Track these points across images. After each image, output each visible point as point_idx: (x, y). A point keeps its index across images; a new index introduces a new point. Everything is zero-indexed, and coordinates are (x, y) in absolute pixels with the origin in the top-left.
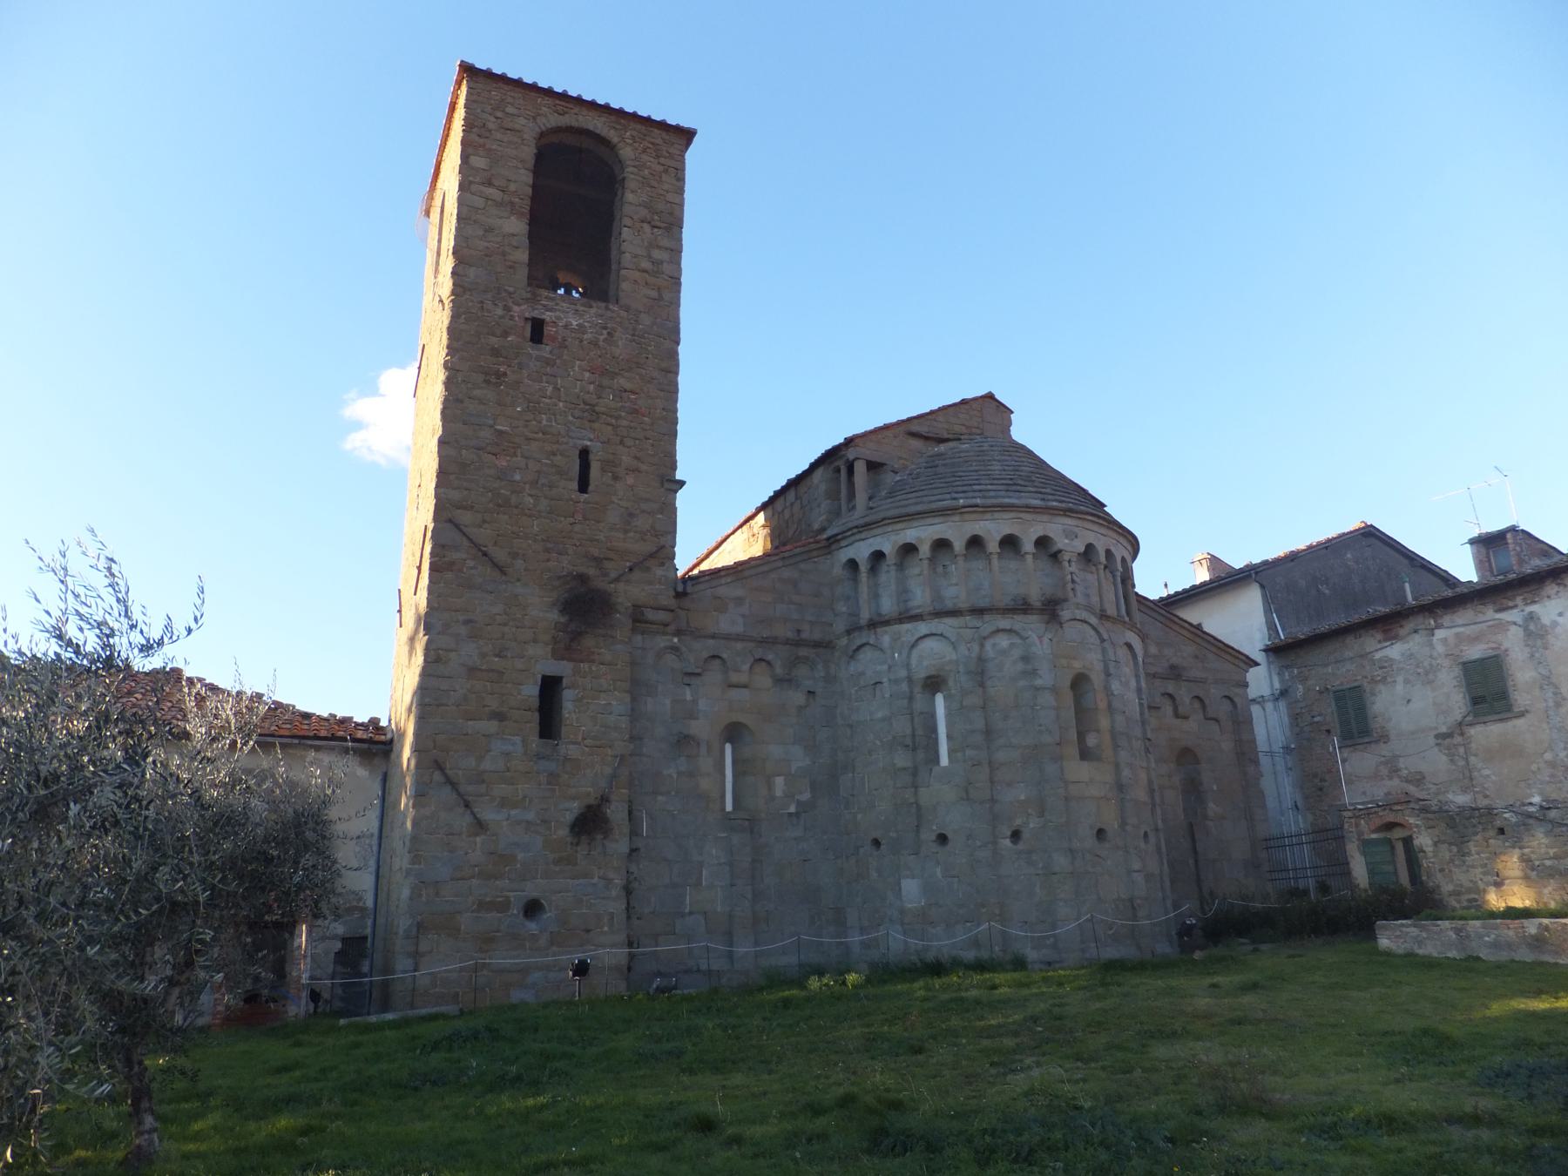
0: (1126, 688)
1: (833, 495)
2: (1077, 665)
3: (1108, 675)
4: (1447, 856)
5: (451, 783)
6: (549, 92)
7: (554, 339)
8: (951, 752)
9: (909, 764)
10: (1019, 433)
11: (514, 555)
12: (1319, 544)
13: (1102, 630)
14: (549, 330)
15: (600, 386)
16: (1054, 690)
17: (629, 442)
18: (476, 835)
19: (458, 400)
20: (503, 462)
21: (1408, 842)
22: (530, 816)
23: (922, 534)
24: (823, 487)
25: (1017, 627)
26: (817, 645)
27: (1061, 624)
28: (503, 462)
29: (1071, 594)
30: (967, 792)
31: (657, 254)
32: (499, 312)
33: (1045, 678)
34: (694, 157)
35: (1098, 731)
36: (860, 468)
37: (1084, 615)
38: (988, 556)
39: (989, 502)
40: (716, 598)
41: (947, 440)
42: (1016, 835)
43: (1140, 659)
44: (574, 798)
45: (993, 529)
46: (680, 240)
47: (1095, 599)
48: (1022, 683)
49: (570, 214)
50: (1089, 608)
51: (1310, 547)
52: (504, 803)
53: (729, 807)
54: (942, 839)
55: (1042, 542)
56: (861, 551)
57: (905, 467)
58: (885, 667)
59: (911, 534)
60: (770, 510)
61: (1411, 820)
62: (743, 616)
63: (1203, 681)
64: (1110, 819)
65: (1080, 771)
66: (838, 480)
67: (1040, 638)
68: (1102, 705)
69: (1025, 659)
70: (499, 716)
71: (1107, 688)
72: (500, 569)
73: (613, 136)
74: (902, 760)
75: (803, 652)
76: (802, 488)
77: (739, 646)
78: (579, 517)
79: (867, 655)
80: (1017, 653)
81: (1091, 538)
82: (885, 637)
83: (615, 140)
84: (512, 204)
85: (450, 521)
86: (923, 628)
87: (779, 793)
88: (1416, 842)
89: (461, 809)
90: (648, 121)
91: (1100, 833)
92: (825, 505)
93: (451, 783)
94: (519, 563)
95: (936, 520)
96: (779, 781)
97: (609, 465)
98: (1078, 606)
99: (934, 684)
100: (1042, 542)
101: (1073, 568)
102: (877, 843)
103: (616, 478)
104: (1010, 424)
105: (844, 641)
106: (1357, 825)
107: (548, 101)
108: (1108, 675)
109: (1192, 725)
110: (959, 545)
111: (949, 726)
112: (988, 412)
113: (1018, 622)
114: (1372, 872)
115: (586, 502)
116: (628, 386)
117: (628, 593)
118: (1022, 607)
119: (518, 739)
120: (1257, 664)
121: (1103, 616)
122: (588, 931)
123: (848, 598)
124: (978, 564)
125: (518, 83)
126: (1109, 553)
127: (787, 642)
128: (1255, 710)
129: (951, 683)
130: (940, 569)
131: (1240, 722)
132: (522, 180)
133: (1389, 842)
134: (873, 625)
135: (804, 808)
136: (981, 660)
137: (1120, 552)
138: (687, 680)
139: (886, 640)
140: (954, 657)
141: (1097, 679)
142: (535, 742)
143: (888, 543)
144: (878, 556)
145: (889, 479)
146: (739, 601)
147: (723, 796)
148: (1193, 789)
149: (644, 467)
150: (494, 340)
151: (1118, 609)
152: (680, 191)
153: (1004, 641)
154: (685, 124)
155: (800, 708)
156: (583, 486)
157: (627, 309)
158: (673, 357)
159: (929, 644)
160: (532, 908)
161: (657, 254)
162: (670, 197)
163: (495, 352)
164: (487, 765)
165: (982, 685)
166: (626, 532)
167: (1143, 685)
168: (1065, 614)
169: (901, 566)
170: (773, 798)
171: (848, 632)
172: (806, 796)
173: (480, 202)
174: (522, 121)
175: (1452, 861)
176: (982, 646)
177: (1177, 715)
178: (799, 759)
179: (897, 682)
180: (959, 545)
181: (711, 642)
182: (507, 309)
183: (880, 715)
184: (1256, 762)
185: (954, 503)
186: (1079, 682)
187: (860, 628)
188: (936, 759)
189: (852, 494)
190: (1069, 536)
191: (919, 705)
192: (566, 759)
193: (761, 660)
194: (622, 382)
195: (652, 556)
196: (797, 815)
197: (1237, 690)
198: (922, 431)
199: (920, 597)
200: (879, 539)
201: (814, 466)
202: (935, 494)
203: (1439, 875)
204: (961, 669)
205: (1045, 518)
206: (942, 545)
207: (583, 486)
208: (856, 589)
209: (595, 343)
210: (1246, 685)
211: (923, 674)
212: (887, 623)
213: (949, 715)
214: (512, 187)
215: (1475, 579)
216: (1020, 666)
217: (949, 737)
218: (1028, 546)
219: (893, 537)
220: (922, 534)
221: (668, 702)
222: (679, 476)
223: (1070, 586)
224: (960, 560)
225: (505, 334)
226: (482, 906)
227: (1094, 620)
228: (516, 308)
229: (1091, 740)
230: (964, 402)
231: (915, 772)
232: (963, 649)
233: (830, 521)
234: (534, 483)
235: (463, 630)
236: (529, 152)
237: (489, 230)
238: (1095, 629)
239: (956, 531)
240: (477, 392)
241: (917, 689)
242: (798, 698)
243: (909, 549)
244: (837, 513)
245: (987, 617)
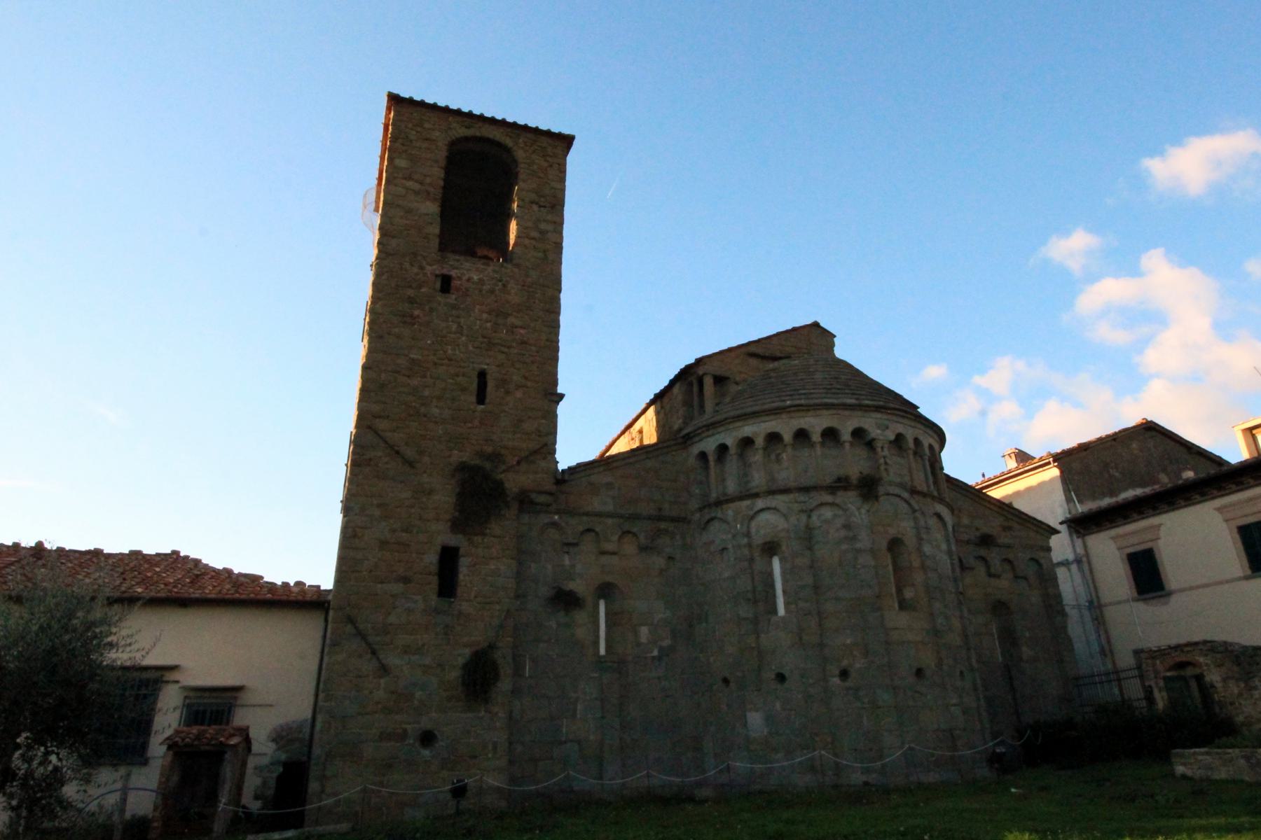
0: (938, 548)
1: (688, 403)
2: (892, 532)
3: (920, 539)
4: (1236, 691)
5: (361, 635)
6: (458, 112)
7: (458, 289)
8: (787, 604)
9: (751, 615)
10: (840, 352)
11: (421, 453)
12: (1108, 436)
13: (913, 502)
14: (456, 283)
15: (496, 324)
16: (873, 552)
17: (517, 366)
18: (380, 677)
19: (381, 337)
20: (415, 382)
21: (1199, 678)
22: (427, 661)
23: (757, 429)
24: (680, 398)
25: (838, 501)
26: (673, 520)
27: (877, 498)
28: (415, 382)
29: (884, 474)
30: (801, 638)
31: (543, 226)
32: (415, 270)
33: (864, 541)
34: (574, 160)
35: (913, 585)
36: (708, 382)
37: (897, 491)
38: (812, 445)
39: (812, 402)
40: (591, 484)
41: (780, 358)
42: (844, 674)
43: (950, 529)
44: (465, 646)
45: (816, 424)
47: (907, 479)
48: (844, 547)
50: (902, 485)
51: (1100, 439)
52: (406, 650)
53: (602, 651)
54: (781, 678)
55: (858, 433)
56: (709, 445)
57: (745, 380)
58: (730, 536)
59: (748, 430)
60: (659, 403)
61: (1201, 660)
62: (613, 498)
63: (1009, 547)
64: (928, 659)
65: (897, 620)
66: (691, 391)
67: (858, 509)
68: (916, 564)
69: (847, 527)
70: (406, 580)
71: (919, 550)
72: (411, 464)
73: (508, 142)
74: (745, 611)
75: (663, 525)
76: (666, 400)
77: (610, 521)
78: (476, 423)
79: (715, 525)
80: (839, 522)
81: (900, 429)
82: (730, 511)
84: (428, 193)
85: (369, 427)
86: (760, 503)
87: (644, 640)
88: (1208, 679)
89: (369, 656)
90: (536, 131)
91: (919, 673)
93: (361, 635)
94: (426, 459)
95: (767, 418)
96: (644, 631)
97: (503, 383)
98: (891, 483)
99: (771, 548)
100: (858, 433)
101: (886, 452)
102: (726, 681)
103: (508, 392)
104: (833, 345)
105: (698, 515)
106: (1154, 665)
107: (459, 119)
108: (920, 539)
109: (1004, 583)
110: (787, 437)
111: (785, 581)
112: (814, 338)
113: (841, 497)
114: (770, 564)
115: (483, 411)
116: (518, 323)
117: (514, 482)
118: (841, 484)
119: (419, 598)
120: (1056, 532)
121: (914, 492)
122: (475, 757)
123: (701, 483)
124: (806, 452)
125: (434, 107)
126: (917, 441)
127: (650, 518)
128: (1061, 573)
129: (784, 548)
130: (773, 457)
131: (1046, 577)
132: (435, 174)
133: (1183, 678)
134: (718, 503)
135: (664, 652)
136: (809, 529)
137: (927, 440)
138: (566, 549)
140: (786, 526)
141: (910, 540)
142: (434, 599)
143: (730, 438)
144: (723, 449)
145: (733, 389)
146: (609, 486)
147: (596, 643)
148: (1009, 637)
149: (529, 384)
150: (410, 292)
151: (928, 487)
152: (562, 180)
153: (828, 513)
154: (566, 131)
155: (661, 571)
156: (481, 399)
157: (518, 266)
159: (764, 517)
160: (427, 738)
163: (411, 301)
164: (392, 619)
165: (810, 549)
166: (514, 433)
167: (954, 548)
168: (881, 490)
169: (741, 455)
170: (639, 644)
171: (700, 510)
172: (666, 643)
173: (400, 190)
174: (437, 134)
175: (1240, 695)
176: (809, 517)
177: (990, 575)
178: (661, 613)
179: (739, 547)
180: (787, 437)
181: (585, 518)
182: (422, 268)
183: (726, 575)
184: (1063, 613)
185: (781, 404)
186: (895, 545)
187: (709, 506)
188: (774, 611)
189: (702, 406)
190: (880, 428)
191: (759, 565)
192: (460, 613)
193: (629, 532)
194: (511, 320)
195: (535, 452)
196: (659, 658)
197: (1042, 554)
198: (760, 353)
199: (758, 479)
200: (723, 435)
201: (673, 383)
202: (779, 406)
203: (1230, 708)
204: (792, 535)
205: (859, 413)
207: (481, 399)
208: (707, 476)
209: (492, 291)
210: (1049, 549)
211: (760, 541)
213: (783, 573)
214: (428, 180)
216: (843, 533)
217: (784, 592)
218: (846, 436)
219: (735, 434)
220: (757, 429)
221: (549, 567)
222: (560, 390)
223: (882, 468)
224: (789, 450)
225: (420, 287)
226: (384, 736)
227: (906, 495)
228: (429, 268)
229: (908, 594)
230: (794, 329)
231: (755, 621)
232: (793, 519)
235: (377, 513)
236: (442, 154)
237: (409, 211)
238: (906, 501)
239: (786, 427)
241: (756, 554)
242: (659, 562)
243: (747, 442)
245: (813, 494)
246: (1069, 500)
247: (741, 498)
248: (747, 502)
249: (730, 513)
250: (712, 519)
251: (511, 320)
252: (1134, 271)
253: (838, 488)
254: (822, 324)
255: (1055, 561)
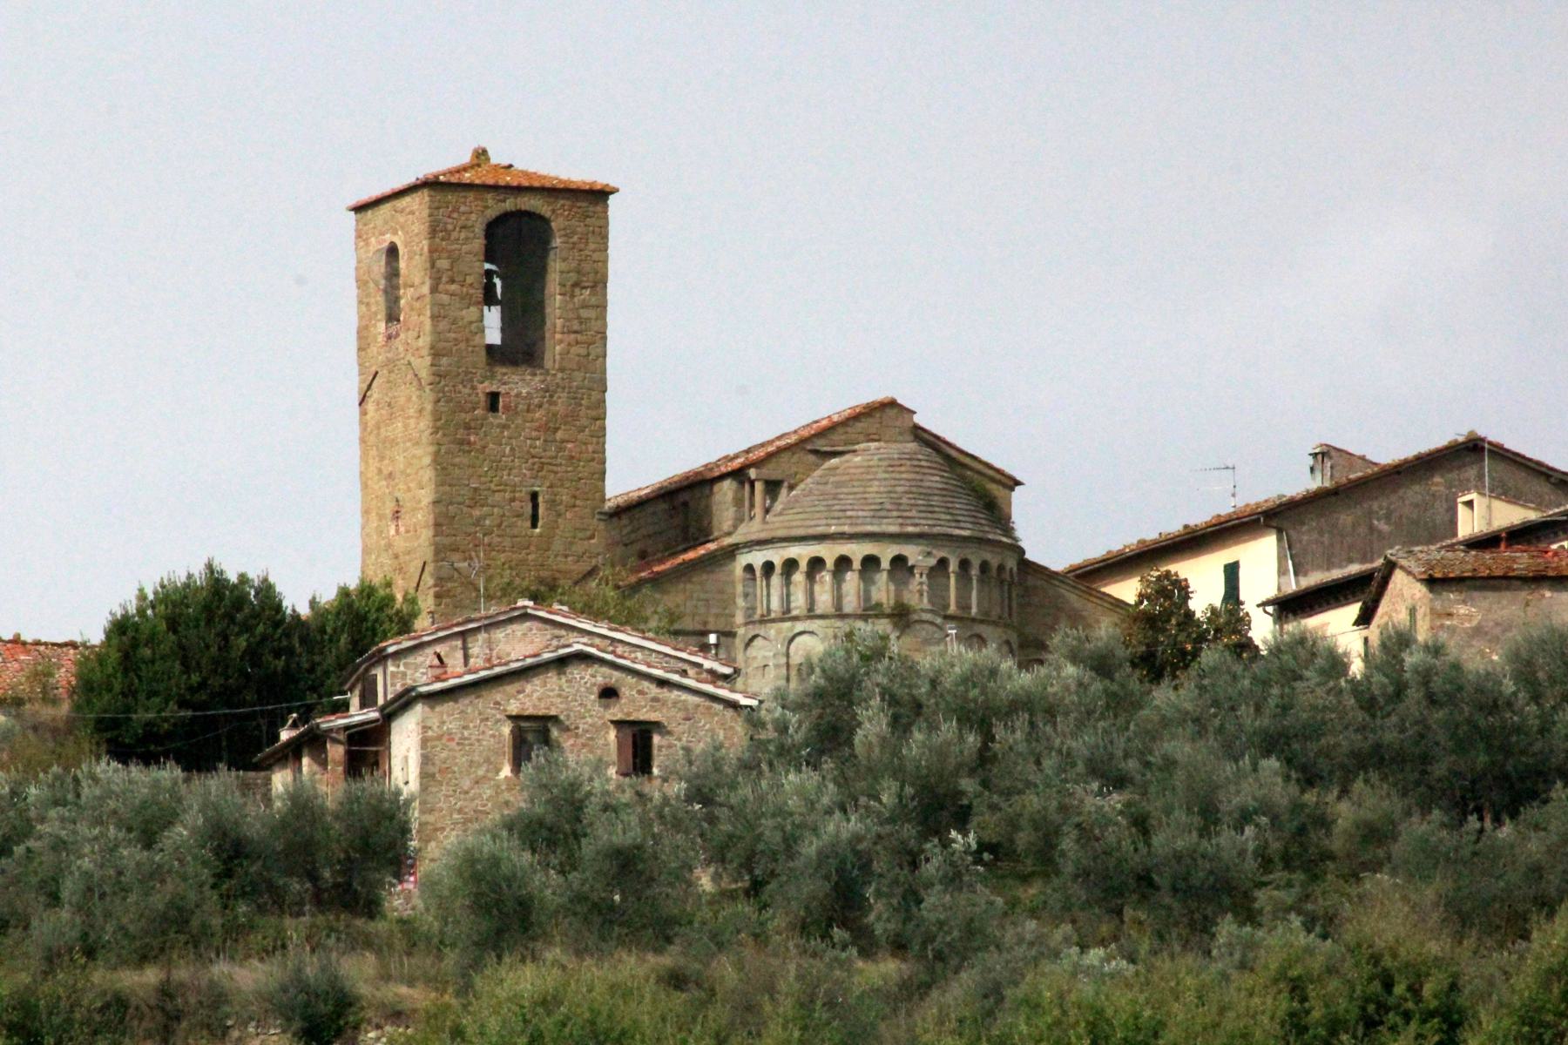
1: (738, 502)
20: (477, 513)
46: (606, 218)
49: (514, 257)
83: (548, 214)
86: (799, 627)
92: (732, 510)
100: (899, 561)
103: (559, 515)
139: (772, 632)
158: (601, 403)
161: (584, 313)
162: (596, 256)
163: (467, 427)
166: (566, 556)
182: (474, 388)
187: (753, 623)
206: (791, 565)
212: (773, 621)
215: (1198, 615)
227: (939, 621)
233: (735, 527)
234: (499, 526)
240: (457, 460)
243: (843, 563)
244: (739, 520)
246: (1282, 572)
247: (782, 620)
248: (788, 624)
249: (772, 632)
250: (755, 636)
251: (559, 435)
252: (1260, 912)
253: (869, 616)
254: (900, 401)
255: (1132, 602)
